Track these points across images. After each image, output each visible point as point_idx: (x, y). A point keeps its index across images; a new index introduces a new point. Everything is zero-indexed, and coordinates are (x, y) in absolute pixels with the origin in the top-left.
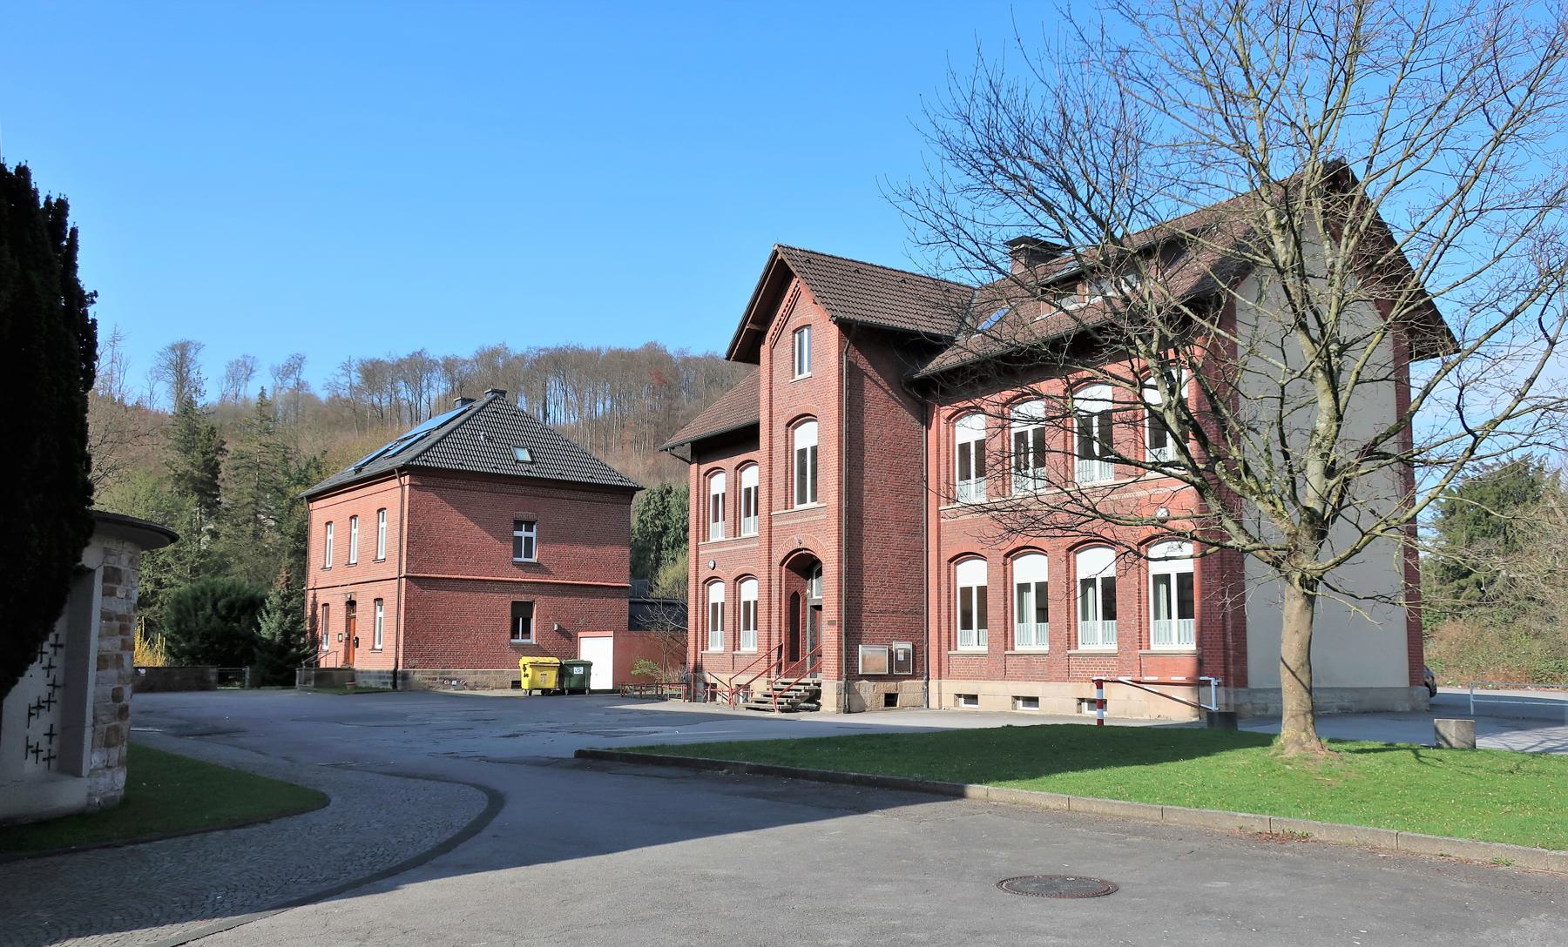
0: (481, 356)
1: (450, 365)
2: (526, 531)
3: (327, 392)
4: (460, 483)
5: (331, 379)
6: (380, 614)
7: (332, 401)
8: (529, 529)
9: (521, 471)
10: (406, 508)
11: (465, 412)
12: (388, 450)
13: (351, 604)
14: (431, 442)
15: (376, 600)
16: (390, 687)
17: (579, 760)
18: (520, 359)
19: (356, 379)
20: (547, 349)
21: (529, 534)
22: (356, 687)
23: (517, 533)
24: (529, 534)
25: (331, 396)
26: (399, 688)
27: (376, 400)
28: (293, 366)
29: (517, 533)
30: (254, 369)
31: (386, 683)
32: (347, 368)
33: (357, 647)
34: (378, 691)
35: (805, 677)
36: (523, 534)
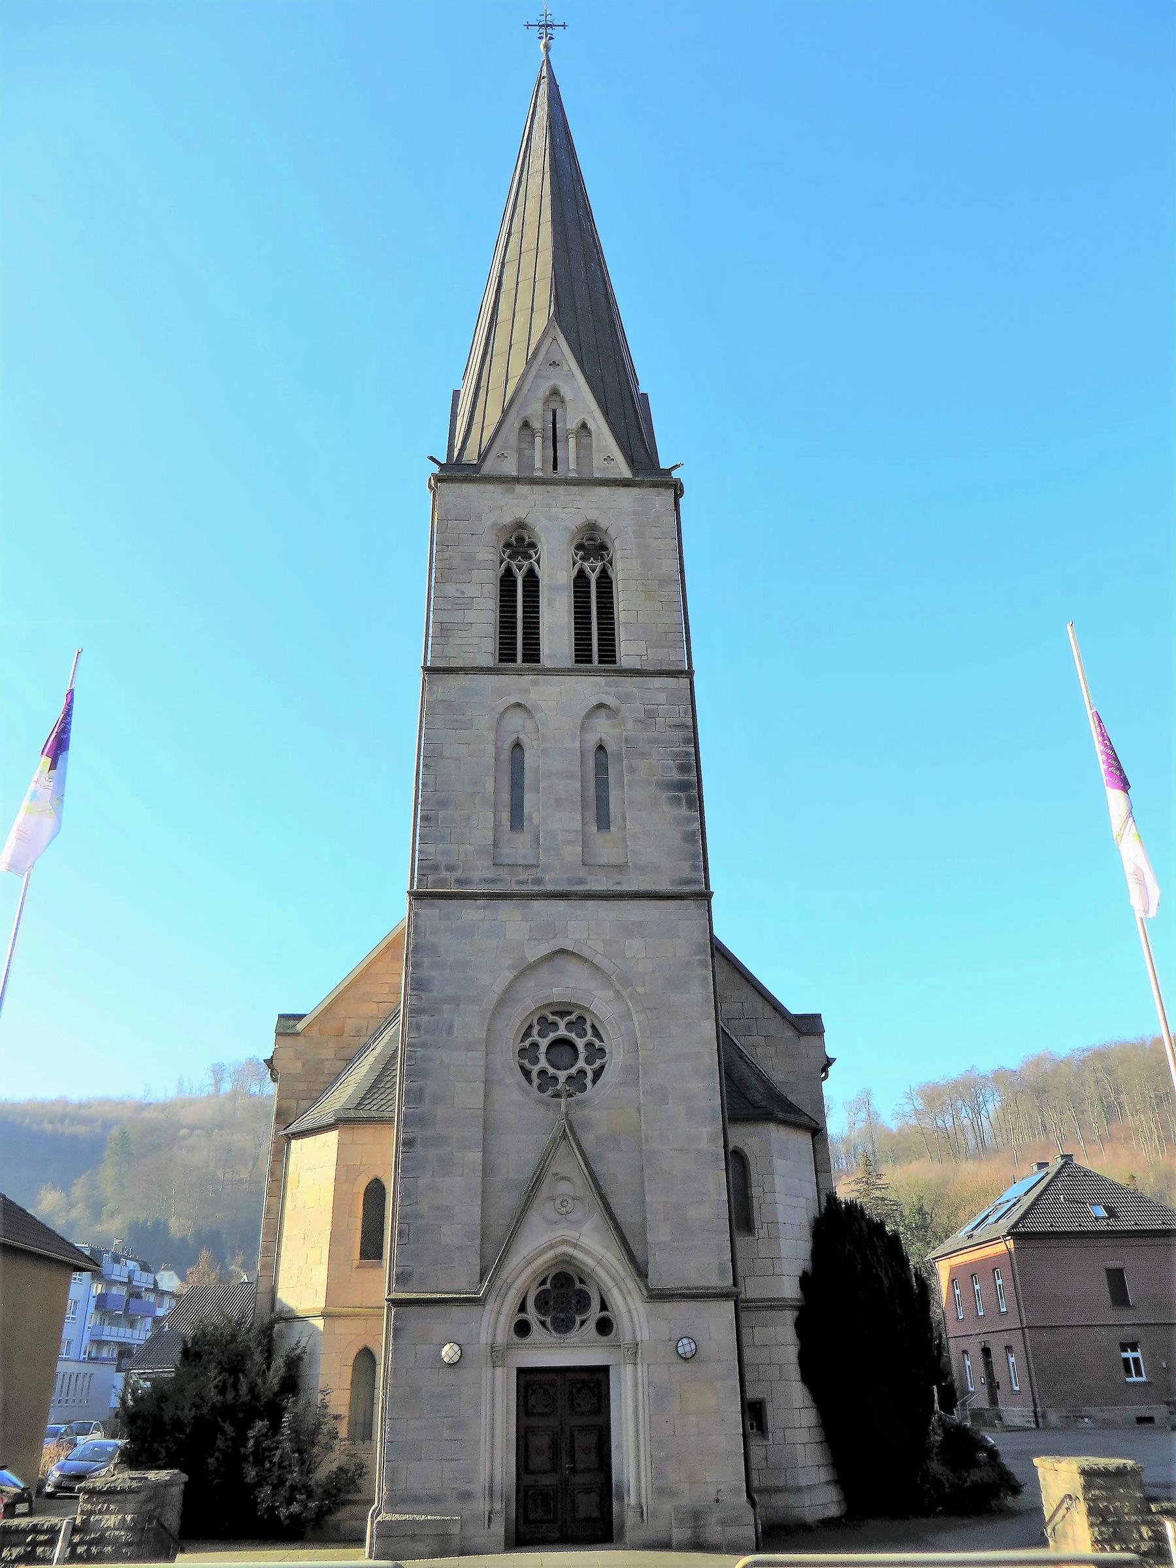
0: (1027, 1065)
1: (1001, 1077)
2: (1136, 1376)
3: (896, 1121)
4: (1053, 1243)
5: (897, 1108)
6: (1012, 1360)
7: (900, 1130)
8: (1134, 1349)
9: (1102, 1226)
10: (436, 523)
11: (1043, 1178)
12: (988, 1216)
13: (986, 1352)
14: (1022, 1211)
15: (1006, 1347)
16: (1034, 1426)
17: (508, 745)
18: (1067, 1061)
19: (919, 1104)
20: (1088, 1049)
21: (1135, 1355)
22: (1003, 1426)
23: (1124, 1355)
24: (1135, 1355)
25: (900, 1124)
26: (1041, 1425)
27: (940, 1123)
28: (865, 1101)
29: (1124, 1355)
30: (831, 1106)
31: (1029, 1422)
32: (909, 1097)
33: (999, 1388)
34: (1026, 1429)
35: (164, 1463)
36: (1129, 1355)
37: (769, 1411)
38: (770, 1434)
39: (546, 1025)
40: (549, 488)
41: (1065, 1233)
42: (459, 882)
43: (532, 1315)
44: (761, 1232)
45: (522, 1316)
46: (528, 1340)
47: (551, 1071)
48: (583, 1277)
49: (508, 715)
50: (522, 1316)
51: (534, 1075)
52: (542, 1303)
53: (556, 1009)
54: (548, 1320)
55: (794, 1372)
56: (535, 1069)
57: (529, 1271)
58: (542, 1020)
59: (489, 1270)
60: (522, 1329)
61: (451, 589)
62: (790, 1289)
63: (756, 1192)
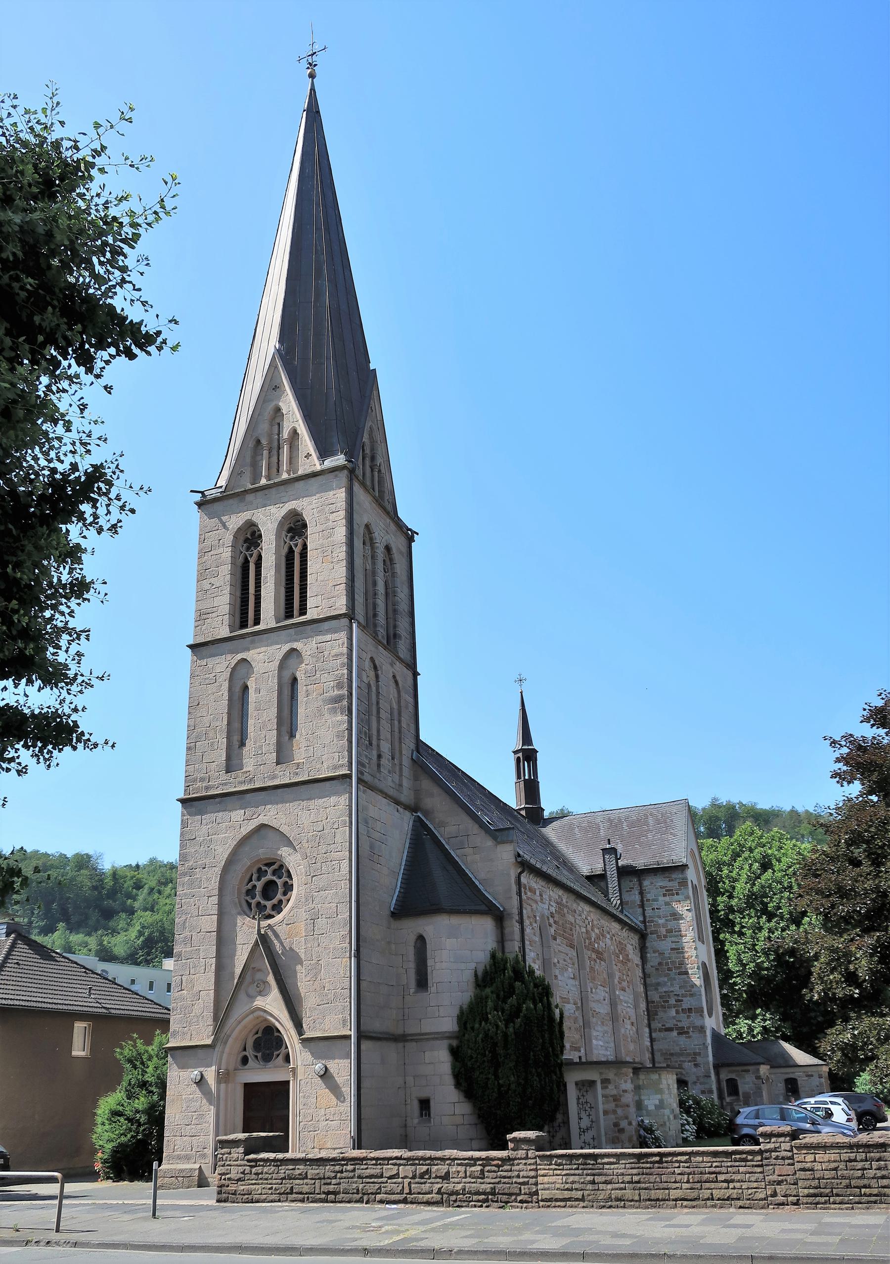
37: (432, 1104)
38: (432, 1120)
39: (261, 873)
40: (266, 492)
41: (312, 1038)
42: (207, 788)
43: (250, 1053)
44: (432, 989)
45: (244, 1053)
46: (246, 1067)
47: (263, 902)
48: (254, 1031)
49: (238, 668)
50: (244, 1053)
51: (253, 906)
52: (257, 1045)
53: (265, 862)
54: (259, 1055)
55: (449, 1080)
56: (253, 902)
57: (240, 1027)
58: (259, 870)
59: (219, 1029)
60: (245, 1060)
61: (206, 585)
62: (448, 1024)
63: (430, 963)
